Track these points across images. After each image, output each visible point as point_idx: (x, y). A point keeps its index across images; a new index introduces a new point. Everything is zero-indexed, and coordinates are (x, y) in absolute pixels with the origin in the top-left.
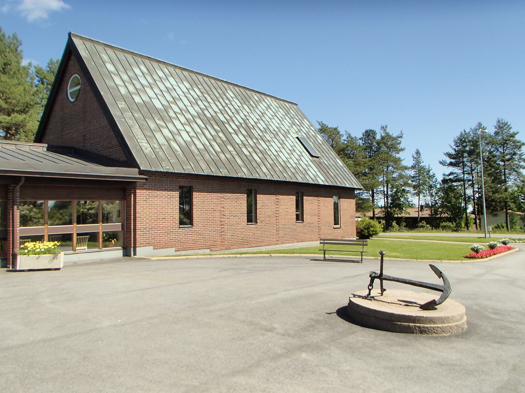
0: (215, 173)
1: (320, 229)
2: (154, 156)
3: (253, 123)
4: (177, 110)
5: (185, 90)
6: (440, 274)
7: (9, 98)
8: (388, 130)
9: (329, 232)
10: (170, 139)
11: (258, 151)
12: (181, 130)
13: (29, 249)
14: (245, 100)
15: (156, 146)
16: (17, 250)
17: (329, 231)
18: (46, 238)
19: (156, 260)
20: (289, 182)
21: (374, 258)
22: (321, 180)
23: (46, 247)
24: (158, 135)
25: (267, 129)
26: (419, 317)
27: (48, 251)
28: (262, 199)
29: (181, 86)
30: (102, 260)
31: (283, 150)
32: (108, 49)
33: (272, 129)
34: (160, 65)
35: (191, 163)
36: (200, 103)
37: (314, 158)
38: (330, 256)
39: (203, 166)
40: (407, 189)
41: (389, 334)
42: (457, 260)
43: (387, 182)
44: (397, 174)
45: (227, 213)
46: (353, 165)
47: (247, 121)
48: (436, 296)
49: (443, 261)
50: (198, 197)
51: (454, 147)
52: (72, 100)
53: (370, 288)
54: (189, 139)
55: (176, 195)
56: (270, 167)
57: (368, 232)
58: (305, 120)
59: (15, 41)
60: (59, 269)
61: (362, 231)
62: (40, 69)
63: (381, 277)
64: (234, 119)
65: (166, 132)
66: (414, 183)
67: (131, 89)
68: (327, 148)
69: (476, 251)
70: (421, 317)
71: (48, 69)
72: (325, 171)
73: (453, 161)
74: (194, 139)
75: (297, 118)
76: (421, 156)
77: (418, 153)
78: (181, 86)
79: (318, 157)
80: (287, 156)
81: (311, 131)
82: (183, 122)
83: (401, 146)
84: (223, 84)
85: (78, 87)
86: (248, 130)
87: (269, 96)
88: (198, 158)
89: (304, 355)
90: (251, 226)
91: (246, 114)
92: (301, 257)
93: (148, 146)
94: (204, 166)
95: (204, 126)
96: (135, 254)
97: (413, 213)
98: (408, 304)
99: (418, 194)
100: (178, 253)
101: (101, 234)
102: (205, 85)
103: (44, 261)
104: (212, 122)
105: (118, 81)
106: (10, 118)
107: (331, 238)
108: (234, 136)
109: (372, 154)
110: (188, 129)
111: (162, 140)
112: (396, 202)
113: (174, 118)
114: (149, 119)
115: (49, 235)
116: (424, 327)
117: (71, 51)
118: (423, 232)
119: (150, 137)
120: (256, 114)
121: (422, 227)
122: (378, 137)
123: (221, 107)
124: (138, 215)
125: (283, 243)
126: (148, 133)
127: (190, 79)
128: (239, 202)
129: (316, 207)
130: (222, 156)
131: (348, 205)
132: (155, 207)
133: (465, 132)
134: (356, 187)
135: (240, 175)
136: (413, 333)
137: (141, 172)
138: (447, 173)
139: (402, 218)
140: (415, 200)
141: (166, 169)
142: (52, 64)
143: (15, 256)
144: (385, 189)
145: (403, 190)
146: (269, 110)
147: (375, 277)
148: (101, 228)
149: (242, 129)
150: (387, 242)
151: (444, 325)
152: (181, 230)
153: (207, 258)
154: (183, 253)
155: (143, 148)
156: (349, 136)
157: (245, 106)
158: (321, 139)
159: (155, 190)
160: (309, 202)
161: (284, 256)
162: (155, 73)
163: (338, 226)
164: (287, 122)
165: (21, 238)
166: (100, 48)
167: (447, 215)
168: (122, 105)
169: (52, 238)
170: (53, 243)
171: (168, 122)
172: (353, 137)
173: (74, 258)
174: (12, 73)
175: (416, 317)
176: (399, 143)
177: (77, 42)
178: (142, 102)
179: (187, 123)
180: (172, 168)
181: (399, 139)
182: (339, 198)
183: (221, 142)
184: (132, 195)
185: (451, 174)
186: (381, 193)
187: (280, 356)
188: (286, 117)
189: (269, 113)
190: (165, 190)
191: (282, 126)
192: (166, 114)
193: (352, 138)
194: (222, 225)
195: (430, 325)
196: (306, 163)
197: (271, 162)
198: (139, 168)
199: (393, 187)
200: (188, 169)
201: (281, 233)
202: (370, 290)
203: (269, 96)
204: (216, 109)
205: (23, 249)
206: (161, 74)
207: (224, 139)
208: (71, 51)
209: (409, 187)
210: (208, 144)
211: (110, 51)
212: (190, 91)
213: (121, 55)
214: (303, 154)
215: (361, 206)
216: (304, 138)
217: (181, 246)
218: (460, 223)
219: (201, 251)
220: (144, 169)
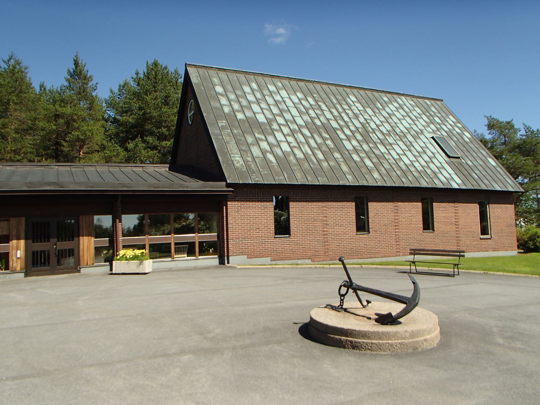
0: (311, 182)
11: (373, 156)
15: (249, 159)
19: (240, 268)
20: (408, 188)
21: (483, 272)
22: (457, 183)
25: (393, 131)
26: (351, 330)
27: (135, 257)
34: (274, 80)
35: (285, 173)
37: (452, 159)
38: (430, 268)
39: (299, 175)
41: (323, 346)
45: (330, 222)
47: (367, 125)
48: (396, 308)
50: (295, 208)
56: (384, 172)
61: (526, 242)
67: (236, 106)
70: (353, 330)
72: (466, 173)
74: (294, 149)
77: (524, 125)
79: (459, 158)
84: (345, 89)
87: (403, 95)
90: (361, 236)
95: (309, 135)
96: (228, 263)
100: (274, 262)
103: (133, 266)
107: (442, 249)
110: (290, 139)
115: (150, 245)
116: (356, 342)
119: (244, 149)
130: (325, 164)
132: (248, 219)
136: (345, 348)
137: (228, 185)
141: (254, 181)
148: (197, 238)
151: (380, 342)
152: (277, 240)
155: (235, 162)
156: (527, 129)
161: (377, 268)
163: (489, 236)
168: (222, 123)
172: (535, 130)
175: (348, 330)
183: (327, 150)
184: (225, 207)
188: (424, 116)
190: (258, 201)
194: (324, 235)
195: (363, 340)
198: (226, 182)
200: (280, 180)
203: (403, 95)
207: (332, 146)
214: (437, 155)
217: (277, 257)
220: (231, 182)
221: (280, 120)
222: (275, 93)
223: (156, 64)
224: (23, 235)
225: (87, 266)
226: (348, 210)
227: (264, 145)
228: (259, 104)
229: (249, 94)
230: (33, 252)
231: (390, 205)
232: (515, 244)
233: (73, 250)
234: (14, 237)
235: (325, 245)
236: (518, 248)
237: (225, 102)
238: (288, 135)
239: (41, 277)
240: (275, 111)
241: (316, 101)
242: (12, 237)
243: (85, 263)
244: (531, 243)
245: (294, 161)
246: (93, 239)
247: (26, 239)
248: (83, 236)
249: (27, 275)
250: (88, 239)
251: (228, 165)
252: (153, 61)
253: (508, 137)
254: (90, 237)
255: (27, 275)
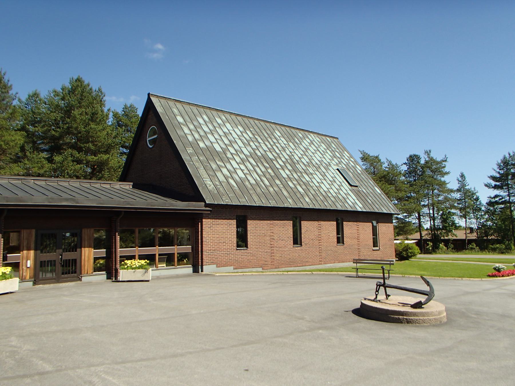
1: (359, 251)
2: (216, 192)
3: (297, 159)
4: (233, 151)
5: (239, 133)
6: (428, 283)
7: (96, 142)
8: (432, 155)
9: (369, 253)
10: (228, 177)
11: (302, 183)
12: (237, 168)
13: (128, 265)
14: (290, 138)
15: (217, 183)
16: (118, 266)
17: (367, 252)
18: (137, 257)
19: (219, 276)
21: (401, 275)
22: (359, 207)
23: (140, 264)
24: (219, 174)
25: (310, 163)
28: (305, 225)
29: (236, 130)
30: (177, 275)
31: (324, 182)
32: (178, 103)
33: (314, 163)
34: (219, 113)
36: (252, 144)
40: (453, 211)
42: (478, 278)
43: (433, 205)
44: (442, 197)
45: (276, 237)
46: (394, 191)
48: (422, 298)
49: (464, 279)
50: (251, 225)
51: (498, 170)
52: (151, 146)
53: (377, 293)
54: (244, 176)
55: (234, 222)
57: (407, 254)
58: (345, 152)
59: (100, 94)
60: (148, 281)
61: (401, 252)
62: (117, 113)
63: (384, 285)
64: (281, 156)
65: (225, 171)
66: (460, 206)
67: (197, 136)
68: (366, 177)
69: (498, 270)
71: (123, 112)
72: (363, 199)
73: (498, 183)
75: (337, 150)
76: (466, 179)
77: (462, 176)
78: (236, 130)
79: (357, 186)
80: (328, 186)
81: (350, 162)
82: (238, 162)
83: (446, 170)
84: (271, 125)
85: (156, 136)
86: (293, 164)
87: (311, 132)
88: (251, 192)
89: (321, 331)
90: (296, 248)
91: (291, 150)
92: (338, 274)
93: (211, 183)
94: (256, 198)
95: (255, 164)
96: (202, 271)
97: (460, 235)
98: (404, 305)
99: (465, 216)
100: (236, 271)
101: (176, 254)
102: (256, 127)
103: (139, 275)
104: (262, 160)
105: (187, 131)
106: (97, 158)
108: (281, 171)
109: (421, 176)
110: (243, 167)
111: (222, 178)
112: (448, 224)
113: (231, 159)
114: (211, 161)
115: (139, 255)
117: (150, 106)
118: (469, 254)
119: (213, 176)
120: (300, 151)
121: (472, 249)
122: (422, 162)
123: (269, 146)
124: (204, 239)
125: (325, 264)
126: (211, 173)
127: (243, 123)
128: (285, 228)
129: (355, 231)
130: (271, 189)
131: (386, 230)
132: (218, 233)
133: (509, 154)
134: (393, 212)
135: (286, 205)
137: (207, 205)
138: (492, 196)
139: (449, 240)
140: (461, 222)
142: (126, 108)
143: (116, 271)
144: (431, 212)
145: (449, 212)
146: (312, 146)
147: (380, 286)
149: (288, 165)
150: (423, 263)
152: (238, 251)
153: (260, 275)
154: (240, 270)
155: (208, 186)
156: (390, 163)
157: (291, 144)
158: (360, 169)
159: (217, 219)
160: (349, 227)
162: (215, 121)
163: (377, 248)
164: (328, 155)
165: (121, 257)
166: (171, 103)
167: (493, 237)
168: (190, 150)
169: (141, 257)
170: (145, 261)
171: (226, 163)
172: (394, 164)
173: (157, 273)
174: (98, 120)
176: (444, 167)
177: (154, 100)
178: (205, 147)
179: (242, 162)
180: (230, 201)
181: (444, 163)
182: (377, 223)
183: (270, 177)
185: (496, 196)
186: (428, 216)
187: (304, 331)
188: (328, 151)
189: (312, 148)
190: (225, 219)
191: (323, 159)
192: (224, 156)
193: (393, 165)
194: (271, 247)
196: (345, 192)
197: (313, 192)
198: (205, 202)
199: (438, 211)
200: (243, 202)
201: (324, 254)
202: (377, 295)
203: (311, 132)
204: (265, 148)
205: (123, 265)
206: (219, 121)
207: (273, 174)
208: (150, 106)
209: (456, 209)
210: (259, 179)
211: (179, 105)
212: (244, 134)
213: (187, 107)
214: (343, 184)
215: (402, 229)
216: (344, 170)
217: (239, 266)
218: (509, 244)
219: (254, 270)
222: (222, 126)
223: (79, 80)
224: (33, 245)
225: (88, 274)
228: (213, 134)
229: (203, 125)
230: (41, 262)
232: (394, 254)
233: (75, 260)
234: (25, 248)
235: (271, 256)
236: (396, 257)
237: (195, 134)
238: (240, 163)
239: (52, 285)
241: (253, 135)
242: (23, 247)
243: (86, 272)
244: (404, 253)
245: (249, 186)
246: (93, 250)
247: (36, 249)
248: (85, 247)
249: (35, 284)
250: (89, 250)
251: (203, 188)
253: (377, 169)
254: (90, 249)
255: (35, 284)
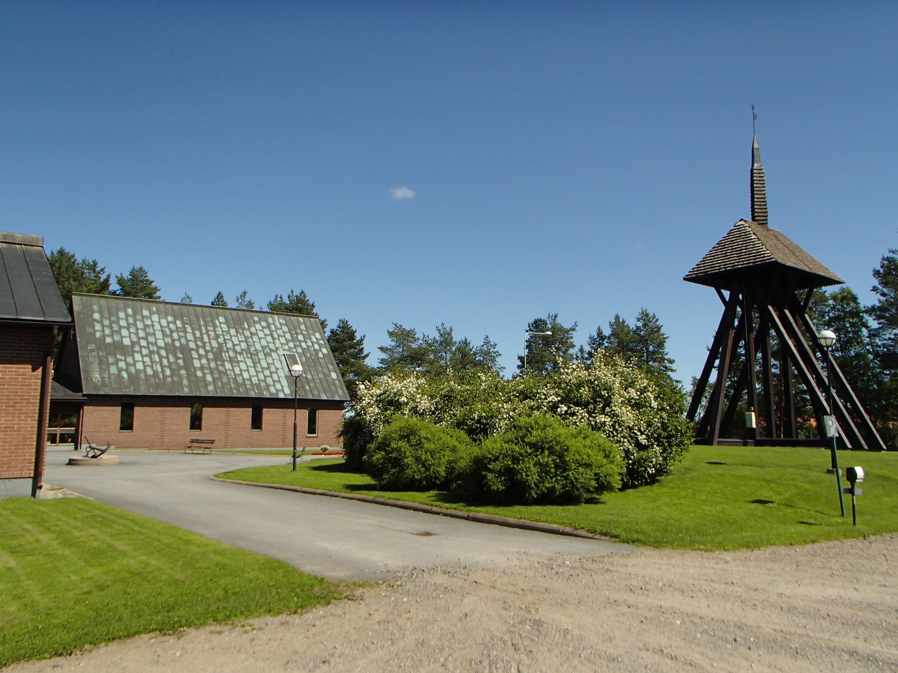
8: (558, 320)
15: (106, 376)
48: (98, 453)
55: (119, 409)
69: (325, 449)
119: (104, 366)
137: (84, 395)
221: (143, 343)
226: (246, 414)
227: (122, 365)
231: (223, 410)
240: (142, 334)
252: (59, 249)
